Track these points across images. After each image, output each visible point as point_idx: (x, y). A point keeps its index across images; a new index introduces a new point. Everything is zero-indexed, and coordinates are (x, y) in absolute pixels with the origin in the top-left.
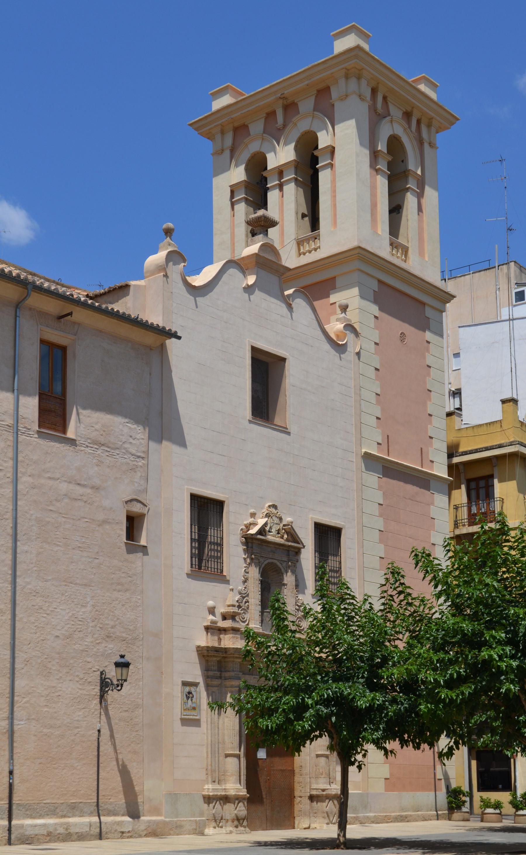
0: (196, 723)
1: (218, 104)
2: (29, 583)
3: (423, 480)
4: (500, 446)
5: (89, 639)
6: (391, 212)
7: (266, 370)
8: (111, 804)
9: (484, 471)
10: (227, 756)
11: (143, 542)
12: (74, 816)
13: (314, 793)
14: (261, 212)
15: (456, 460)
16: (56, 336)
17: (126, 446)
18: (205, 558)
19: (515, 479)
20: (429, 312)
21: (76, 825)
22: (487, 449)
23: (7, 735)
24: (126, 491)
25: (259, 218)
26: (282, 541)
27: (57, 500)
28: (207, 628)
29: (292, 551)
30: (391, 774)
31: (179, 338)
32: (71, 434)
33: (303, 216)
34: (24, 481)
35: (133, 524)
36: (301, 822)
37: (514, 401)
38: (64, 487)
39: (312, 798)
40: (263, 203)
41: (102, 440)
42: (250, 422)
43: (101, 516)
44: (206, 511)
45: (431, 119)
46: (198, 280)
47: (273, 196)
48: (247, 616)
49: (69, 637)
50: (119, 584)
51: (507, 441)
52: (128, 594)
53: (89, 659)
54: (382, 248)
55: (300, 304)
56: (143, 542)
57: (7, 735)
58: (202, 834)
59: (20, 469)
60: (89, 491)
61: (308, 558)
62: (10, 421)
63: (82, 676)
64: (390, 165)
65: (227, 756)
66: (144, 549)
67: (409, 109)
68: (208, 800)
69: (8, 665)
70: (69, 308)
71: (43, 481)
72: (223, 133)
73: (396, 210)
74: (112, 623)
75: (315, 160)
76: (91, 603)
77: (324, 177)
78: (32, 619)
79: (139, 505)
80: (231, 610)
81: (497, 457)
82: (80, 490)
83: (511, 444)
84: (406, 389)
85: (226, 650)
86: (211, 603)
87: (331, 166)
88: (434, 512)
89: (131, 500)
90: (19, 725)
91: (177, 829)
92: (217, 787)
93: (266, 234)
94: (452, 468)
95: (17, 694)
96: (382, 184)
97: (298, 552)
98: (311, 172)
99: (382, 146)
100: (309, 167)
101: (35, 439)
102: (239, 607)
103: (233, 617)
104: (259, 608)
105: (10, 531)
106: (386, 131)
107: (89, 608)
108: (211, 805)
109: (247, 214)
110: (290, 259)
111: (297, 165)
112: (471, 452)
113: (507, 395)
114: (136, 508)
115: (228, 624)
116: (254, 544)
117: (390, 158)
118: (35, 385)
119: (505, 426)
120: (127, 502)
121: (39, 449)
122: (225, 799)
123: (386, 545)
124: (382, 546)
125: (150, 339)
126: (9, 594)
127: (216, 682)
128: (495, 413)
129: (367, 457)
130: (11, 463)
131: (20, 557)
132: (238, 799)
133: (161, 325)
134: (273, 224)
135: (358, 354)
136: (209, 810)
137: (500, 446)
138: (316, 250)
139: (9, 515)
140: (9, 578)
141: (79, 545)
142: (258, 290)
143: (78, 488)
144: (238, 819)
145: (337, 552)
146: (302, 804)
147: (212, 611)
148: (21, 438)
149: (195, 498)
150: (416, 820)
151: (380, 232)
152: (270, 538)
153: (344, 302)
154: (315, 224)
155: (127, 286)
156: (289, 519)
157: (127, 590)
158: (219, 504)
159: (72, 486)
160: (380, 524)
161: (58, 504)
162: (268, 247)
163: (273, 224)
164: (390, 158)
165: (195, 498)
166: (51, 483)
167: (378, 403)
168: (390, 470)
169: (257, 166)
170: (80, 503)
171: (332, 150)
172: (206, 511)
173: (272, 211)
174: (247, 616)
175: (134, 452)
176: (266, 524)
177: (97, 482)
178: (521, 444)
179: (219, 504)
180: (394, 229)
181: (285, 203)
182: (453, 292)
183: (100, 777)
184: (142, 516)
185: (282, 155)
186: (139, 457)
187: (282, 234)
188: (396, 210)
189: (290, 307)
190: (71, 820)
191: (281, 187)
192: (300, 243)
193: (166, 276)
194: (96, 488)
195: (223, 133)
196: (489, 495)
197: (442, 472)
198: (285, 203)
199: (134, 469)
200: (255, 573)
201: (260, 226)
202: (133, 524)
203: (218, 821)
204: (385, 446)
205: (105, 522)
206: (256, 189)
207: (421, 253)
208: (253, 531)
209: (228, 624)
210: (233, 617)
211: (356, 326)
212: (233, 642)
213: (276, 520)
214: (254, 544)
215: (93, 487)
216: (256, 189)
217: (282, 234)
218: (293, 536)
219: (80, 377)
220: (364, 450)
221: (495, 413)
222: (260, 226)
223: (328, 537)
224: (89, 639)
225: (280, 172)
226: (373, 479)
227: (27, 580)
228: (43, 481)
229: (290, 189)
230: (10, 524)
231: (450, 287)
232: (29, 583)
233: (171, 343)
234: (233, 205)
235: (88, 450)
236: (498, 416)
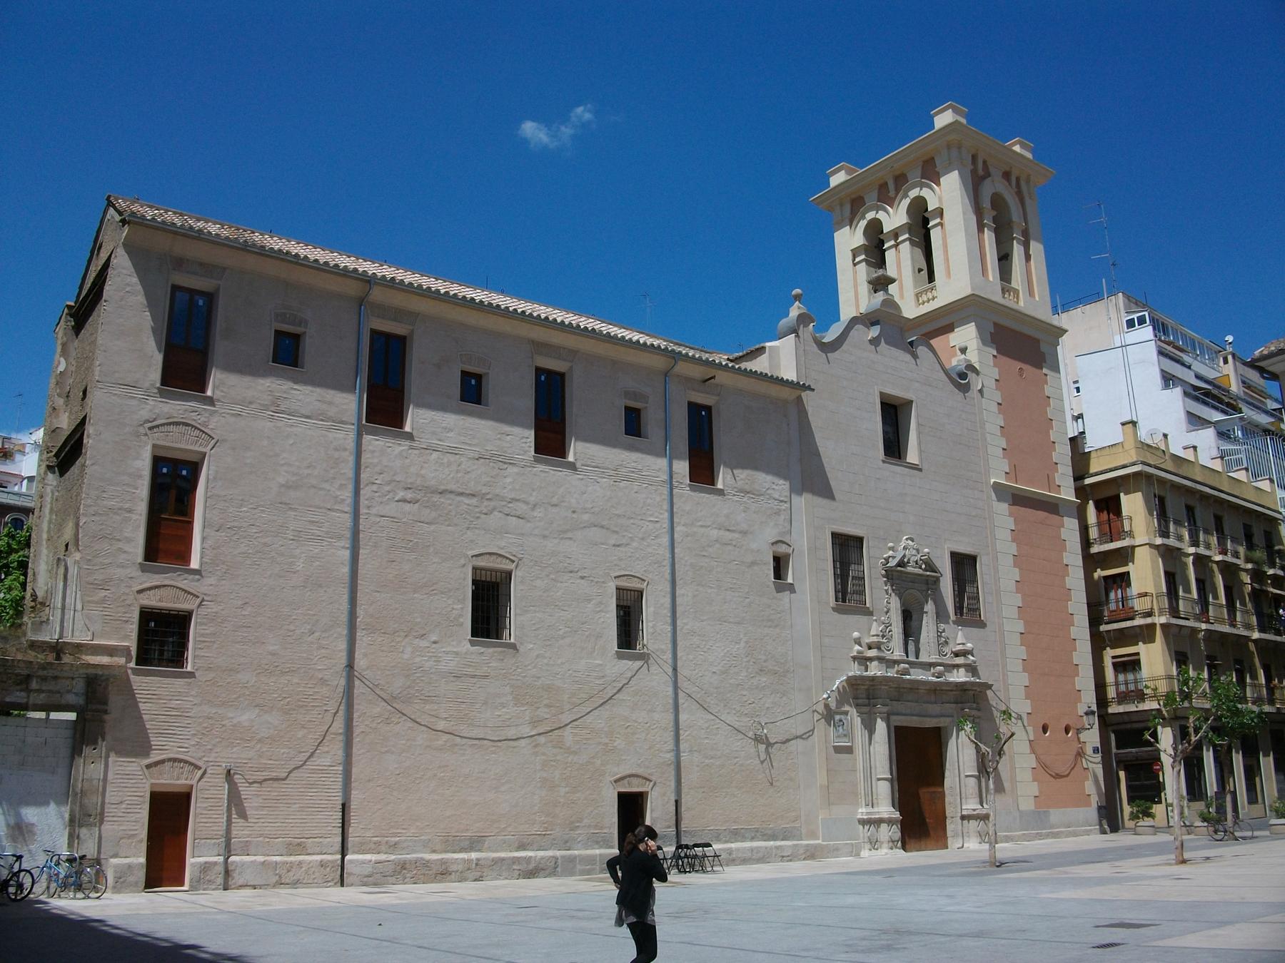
6: (1000, 260)
9: (1109, 493)
10: (879, 779)
11: (790, 580)
13: (965, 813)
16: (701, 399)
18: (847, 591)
20: (1044, 348)
21: (738, 850)
22: (1111, 470)
24: (771, 534)
26: (921, 572)
27: (709, 546)
30: (1040, 792)
32: (720, 485)
34: (679, 529)
35: (780, 565)
36: (954, 843)
37: (1134, 423)
38: (714, 533)
39: (963, 818)
40: (881, 263)
41: (747, 488)
44: (847, 549)
45: (1029, 176)
46: (830, 336)
47: (890, 256)
48: (890, 645)
54: (993, 293)
56: (790, 580)
57: (672, 767)
59: (676, 520)
60: (737, 535)
61: (947, 586)
62: (665, 477)
64: (995, 220)
65: (879, 779)
66: (791, 588)
68: (863, 822)
69: (671, 701)
70: (711, 372)
72: (842, 205)
73: (1004, 258)
75: (926, 221)
77: (935, 235)
78: (691, 657)
79: (784, 546)
82: (729, 535)
83: (1134, 464)
84: (1029, 418)
86: (856, 634)
87: (941, 224)
88: (1064, 534)
89: (777, 542)
90: (684, 757)
93: (886, 291)
94: (1081, 491)
95: (342, 543)
97: (937, 580)
99: (986, 204)
100: (921, 226)
103: (878, 646)
104: (902, 636)
105: (668, 576)
106: (988, 190)
107: (742, 644)
109: (868, 274)
110: (910, 310)
111: (909, 228)
113: (1128, 418)
114: (782, 549)
116: (896, 576)
117: (994, 213)
118: (684, 447)
121: (691, 499)
122: (878, 822)
125: (786, 393)
127: (865, 709)
129: (997, 487)
130: (666, 515)
131: (679, 600)
132: (890, 822)
134: (892, 281)
135: (981, 391)
137: (1124, 467)
139: (667, 563)
141: (294, 429)
142: (886, 343)
145: (974, 580)
148: (675, 491)
149: (835, 535)
150: (1067, 836)
152: (909, 569)
153: (963, 345)
154: (931, 278)
155: (764, 348)
159: (722, 532)
163: (892, 281)
164: (994, 213)
165: (835, 535)
166: (703, 530)
167: (1003, 435)
168: (1020, 500)
169: (874, 230)
170: (730, 548)
171: (940, 212)
172: (847, 549)
173: (891, 271)
176: (904, 556)
177: (744, 526)
180: (1005, 274)
181: (901, 259)
182: (1065, 326)
183: (361, 571)
184: (787, 556)
185: (894, 218)
187: (901, 288)
188: (1004, 258)
189: (915, 356)
192: (918, 296)
193: (797, 336)
194: (744, 533)
195: (842, 205)
196: (1118, 512)
197: (1068, 493)
198: (901, 259)
199: (778, 513)
200: (895, 604)
201: (880, 284)
202: (780, 565)
203: (874, 844)
205: (753, 563)
206: (875, 250)
207: (1031, 293)
208: (893, 563)
210: (878, 646)
214: (896, 576)
216: (875, 250)
217: (901, 288)
218: (930, 566)
222: (880, 284)
223: (964, 565)
225: (895, 234)
226: (1004, 507)
229: (906, 248)
230: (668, 570)
231: (1056, 321)
233: (806, 395)
234: (855, 265)
235: (735, 498)
236: (1118, 438)
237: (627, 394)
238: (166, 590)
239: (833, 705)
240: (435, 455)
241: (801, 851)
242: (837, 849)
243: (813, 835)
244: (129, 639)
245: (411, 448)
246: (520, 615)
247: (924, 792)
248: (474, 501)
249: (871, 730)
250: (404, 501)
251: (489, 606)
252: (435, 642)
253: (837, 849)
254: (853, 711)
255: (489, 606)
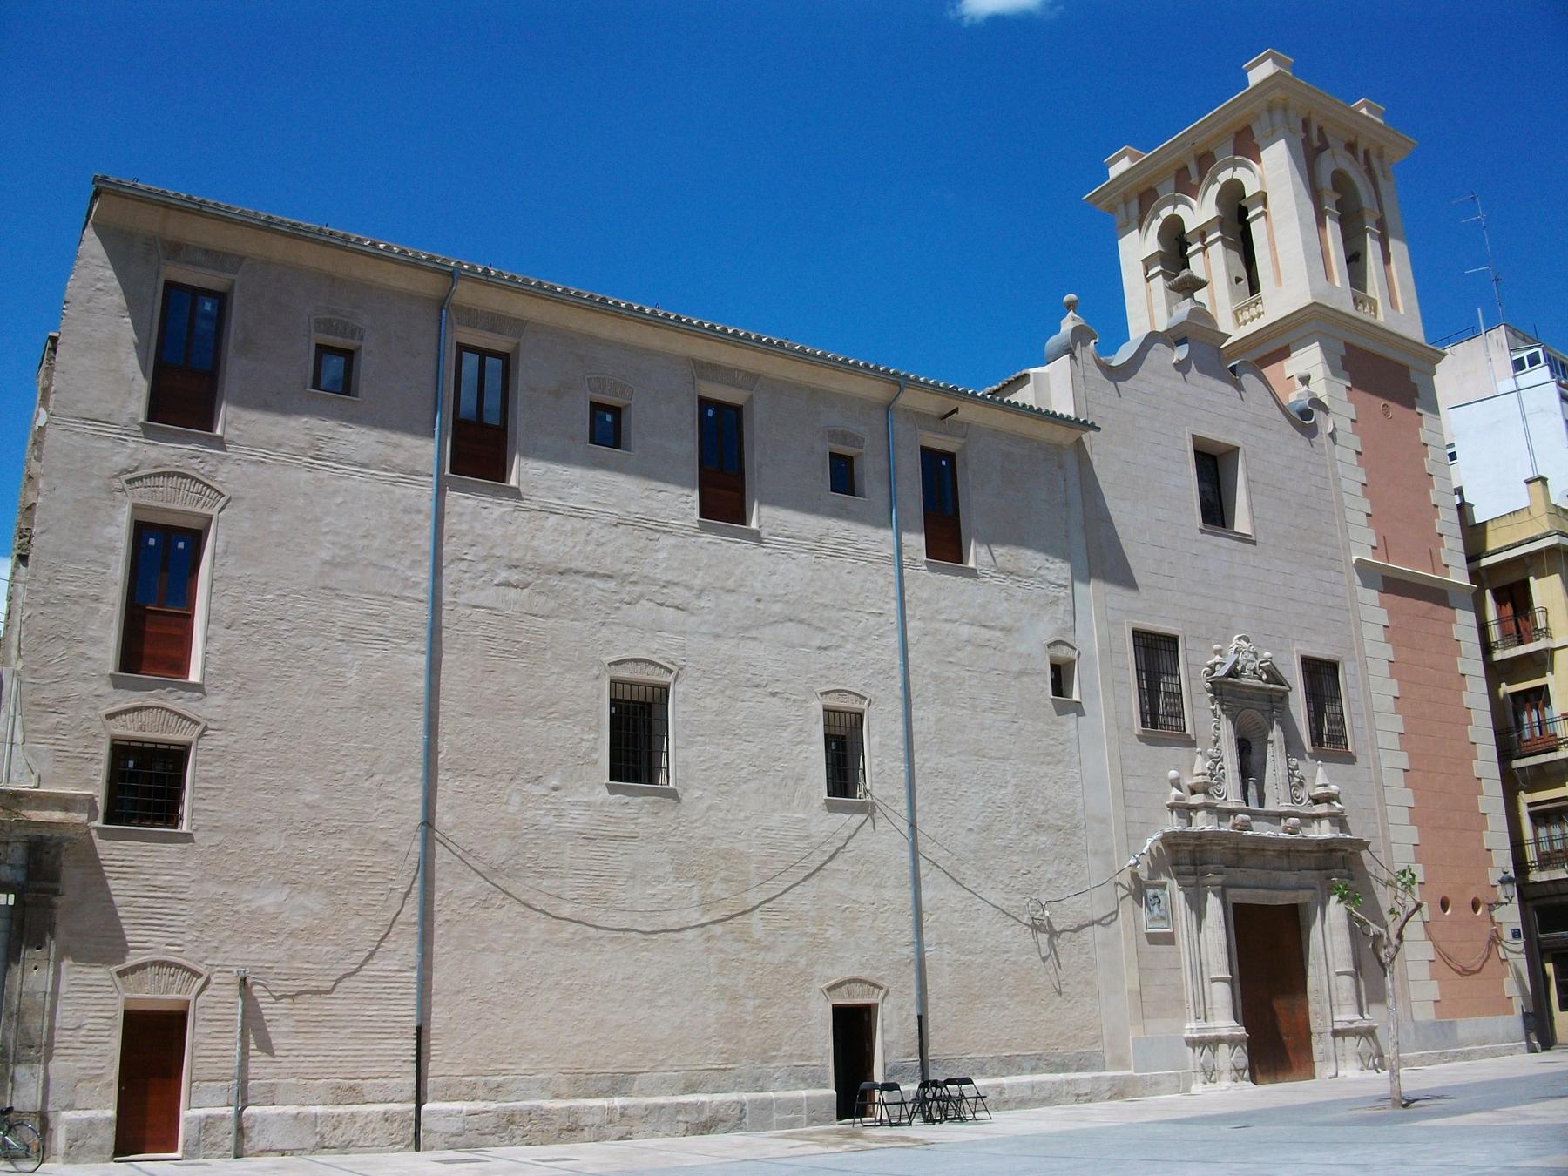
0: (1169, 939)
1: (1115, 171)
2: (927, 760)
3: (1438, 595)
4: (1533, 540)
5: (1014, 831)
7: (1214, 467)
8: (1059, 1055)
9: (1515, 577)
11: (1076, 697)
12: (1009, 1074)
14: (1185, 273)
15: (1485, 562)
17: (1041, 572)
18: (1158, 713)
19: (1526, 583)
21: (1012, 1087)
23: (913, 967)
24: (1046, 631)
25: (1184, 280)
26: (1261, 684)
28: (1172, 807)
29: (1275, 701)
31: (1099, 429)
33: (1238, 280)
35: (1060, 677)
36: (1323, 1070)
38: (965, 631)
41: (1010, 567)
42: (1202, 531)
43: (1016, 666)
48: (1223, 788)
49: (986, 829)
50: (1047, 755)
51: (1536, 532)
52: (1060, 768)
53: (1015, 858)
55: (1248, 379)
56: (1076, 697)
58: (1187, 1090)
60: (999, 634)
61: (1298, 704)
63: (1007, 881)
64: (1339, 205)
65: (1213, 980)
67: (1352, 139)
68: (1193, 1043)
69: (908, 872)
71: (937, 625)
72: (1126, 202)
73: (1355, 259)
74: (1042, 807)
75: (1244, 211)
76: (1013, 782)
78: (935, 807)
80: (1200, 779)
81: (1538, 553)
83: (1546, 536)
84: (1405, 476)
85: (1200, 835)
86: (1173, 774)
90: (930, 953)
91: (1153, 1086)
92: (1202, 1024)
94: (1474, 575)
96: (1332, 229)
97: (1284, 697)
98: (1240, 228)
99: (1326, 182)
100: (1237, 221)
101: (923, 571)
102: (1212, 776)
103: (1205, 789)
105: (899, 692)
106: (1326, 166)
107: (1010, 789)
108: (1198, 1050)
111: (1220, 223)
112: (1501, 550)
114: (1063, 653)
115: (1198, 799)
116: (1226, 690)
117: (1338, 196)
119: (1535, 512)
120: (1049, 646)
123: (1400, 680)
124: (1395, 682)
125: (1062, 435)
126: (903, 775)
127: (1191, 880)
128: (1521, 497)
130: (894, 605)
131: (916, 727)
133: (1073, 416)
135: (1332, 435)
136: (1193, 1057)
137: (1533, 540)
138: (1259, 315)
140: (902, 754)
143: (983, 630)
144: (1237, 1070)
146: (1321, 1046)
147: (1176, 783)
149: (1137, 634)
151: (1338, 284)
152: (1245, 680)
153: (1303, 372)
154: (1254, 288)
156: (1267, 654)
157: (1059, 762)
158: (1173, 641)
159: (975, 629)
160: (1388, 653)
161: (959, 654)
162: (1199, 313)
163: (1201, 284)
164: (1338, 196)
165: (1137, 634)
166: (948, 626)
167: (1366, 495)
170: (988, 651)
171: (1262, 198)
172: (1155, 653)
174: (1223, 788)
175: (1052, 579)
176: (1237, 662)
177: (1007, 621)
178: (1560, 534)
179: (1173, 641)
181: (1212, 263)
184: (1070, 664)
185: (1199, 212)
186: (1060, 586)
187: (1212, 297)
188: (1355, 259)
190: (1005, 1080)
191: (1204, 249)
195: (1126, 202)
197: (1459, 575)
198: (1212, 263)
199: (1055, 602)
200: (1227, 730)
202: (1060, 677)
203: (1210, 1074)
204: (1382, 551)
205: (1022, 673)
208: (1221, 672)
209: (1198, 799)
210: (1205, 789)
211: (1325, 400)
212: (1202, 823)
213: (1251, 657)
214: (1226, 690)
215: (1002, 629)
218: (1274, 676)
219: (976, 498)
220: (1354, 558)
221: (1521, 497)
224: (1014, 831)
225: (1202, 233)
227: (926, 756)
228: (937, 625)
229: (1217, 250)
230: (899, 682)
232: (927, 760)
233: (1088, 438)
234: (1148, 280)
235: (993, 581)
236: (1524, 502)
237: (833, 435)
238: (152, 715)
239: (1144, 875)
240: (553, 519)
241: (1105, 1087)
242: (1157, 1083)
243: (1121, 1062)
244: (92, 782)
245: (517, 509)
246: (683, 748)
247: (1279, 1004)
248: (611, 585)
249: (1200, 912)
250: (508, 584)
251: (636, 737)
252: (555, 789)
253: (1157, 1083)
254: (1173, 884)
255: (636, 737)
